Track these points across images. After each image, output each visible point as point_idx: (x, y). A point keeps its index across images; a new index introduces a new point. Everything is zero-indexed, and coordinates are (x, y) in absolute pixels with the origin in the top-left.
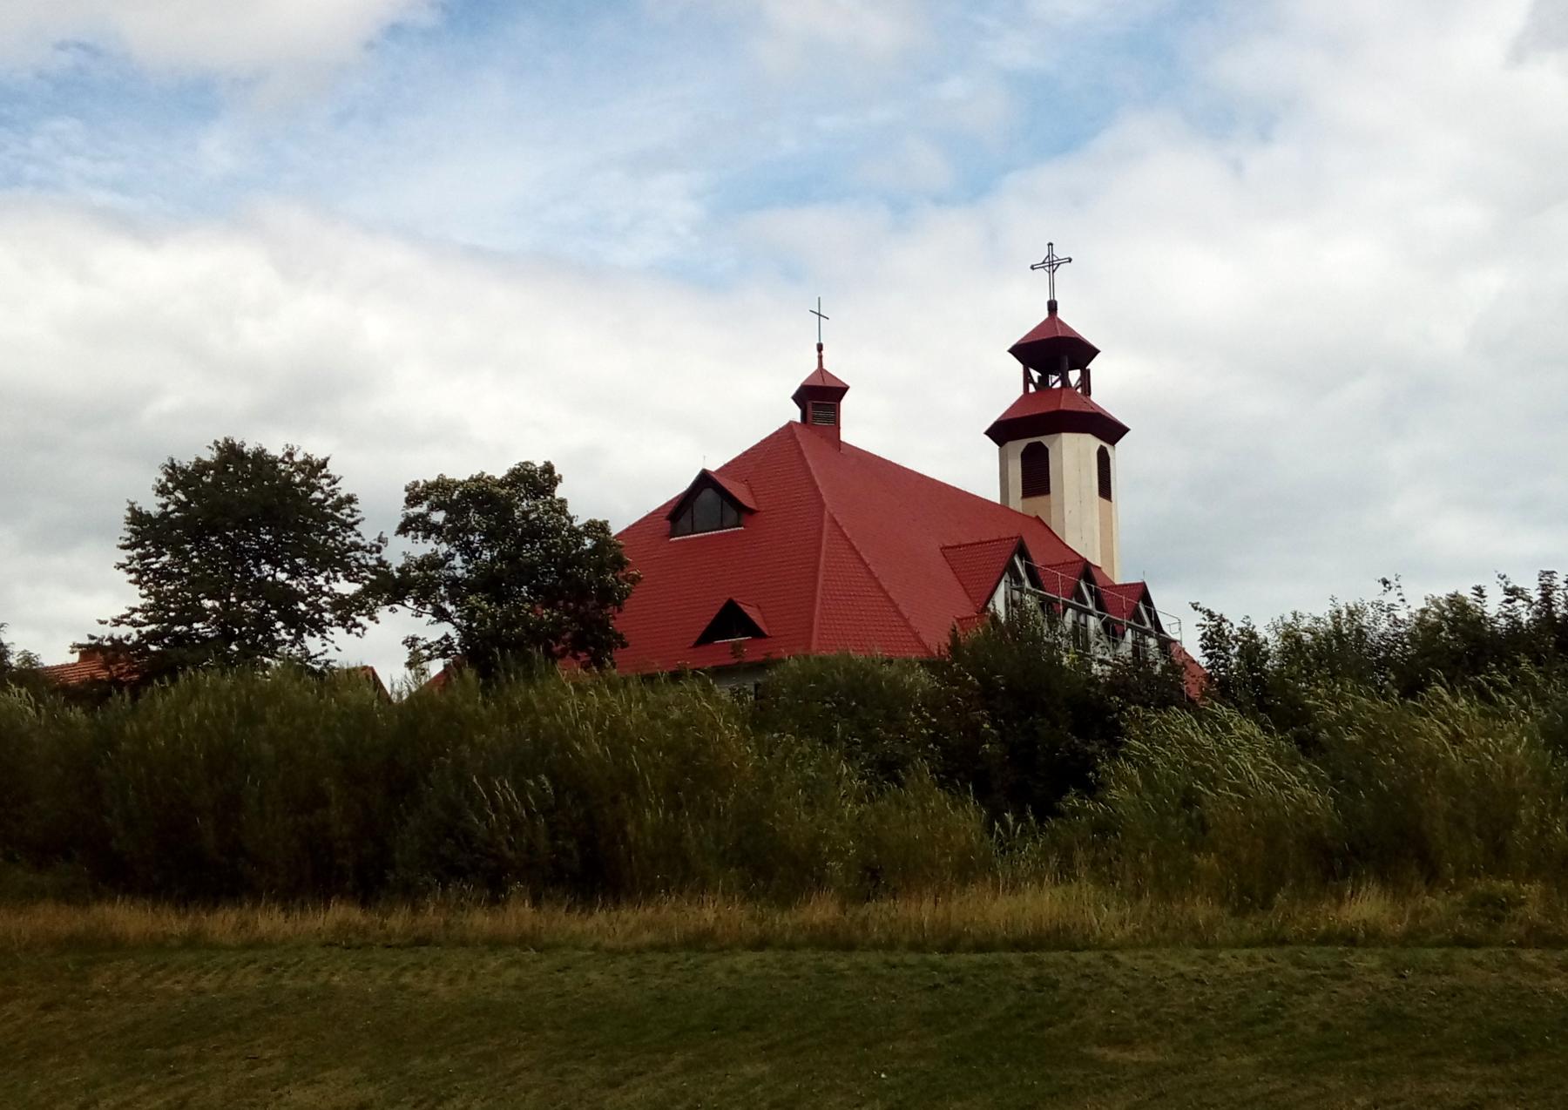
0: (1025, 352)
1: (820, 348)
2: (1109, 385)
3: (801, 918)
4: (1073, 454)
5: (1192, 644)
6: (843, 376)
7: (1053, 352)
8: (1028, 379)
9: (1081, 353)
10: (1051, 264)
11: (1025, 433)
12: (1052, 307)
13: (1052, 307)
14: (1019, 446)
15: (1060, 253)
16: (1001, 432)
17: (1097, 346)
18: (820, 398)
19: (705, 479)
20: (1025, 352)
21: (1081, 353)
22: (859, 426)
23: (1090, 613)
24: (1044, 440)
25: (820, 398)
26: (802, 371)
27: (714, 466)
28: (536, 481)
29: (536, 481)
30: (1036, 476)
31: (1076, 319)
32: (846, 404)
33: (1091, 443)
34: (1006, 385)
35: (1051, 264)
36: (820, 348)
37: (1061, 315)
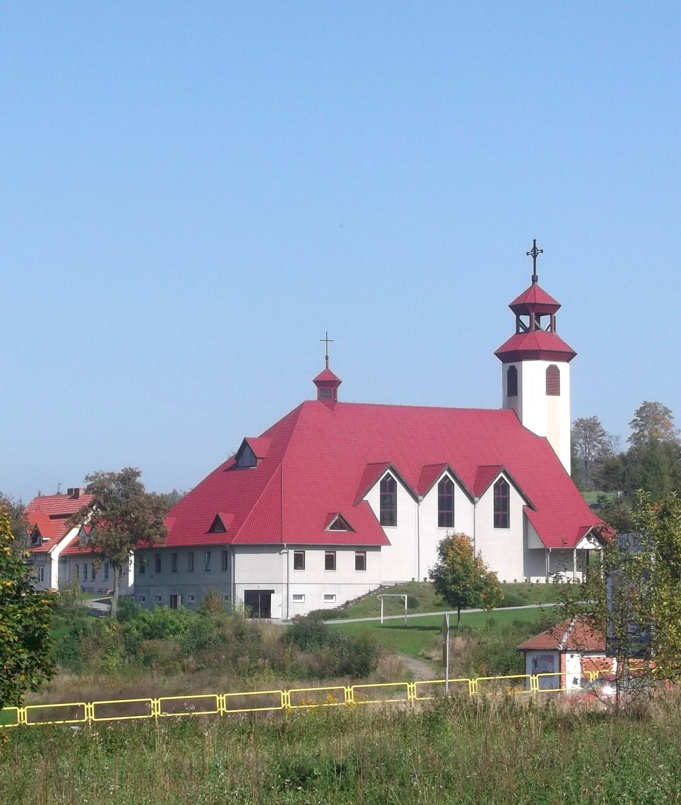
0: (519, 308)
1: (327, 358)
2: (567, 327)
4: (533, 372)
6: (339, 375)
7: (533, 306)
8: (519, 323)
9: (551, 308)
10: (535, 253)
11: (512, 356)
12: (535, 279)
13: (535, 279)
15: (539, 247)
17: (557, 298)
18: (327, 384)
20: (519, 308)
21: (551, 308)
22: (343, 395)
23: (83, 525)
25: (327, 384)
26: (318, 370)
27: (255, 432)
28: (128, 478)
29: (128, 478)
31: (550, 287)
32: (340, 389)
34: (505, 327)
35: (535, 253)
36: (327, 358)
37: (540, 283)
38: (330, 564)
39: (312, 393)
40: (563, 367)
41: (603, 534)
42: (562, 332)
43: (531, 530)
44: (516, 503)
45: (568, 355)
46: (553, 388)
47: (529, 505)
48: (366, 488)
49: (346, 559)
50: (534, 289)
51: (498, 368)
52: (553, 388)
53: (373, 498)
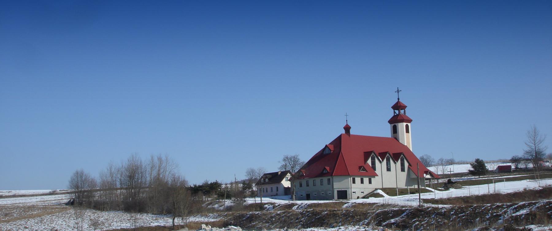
2: (409, 113)
3: (539, 228)
4: (402, 126)
5: (246, 199)
7: (398, 106)
8: (395, 112)
9: (404, 107)
10: (398, 91)
11: (395, 121)
12: (398, 99)
13: (398, 99)
14: (393, 125)
15: (399, 89)
16: (390, 122)
17: (406, 104)
18: (347, 129)
19: (326, 146)
21: (404, 107)
22: (352, 132)
24: (396, 124)
25: (347, 129)
27: (328, 144)
30: (395, 130)
31: (403, 101)
33: (405, 124)
34: (391, 114)
35: (398, 91)
38: (362, 182)
39: (343, 132)
40: (409, 124)
41: (39, 219)
42: (407, 114)
43: (411, 172)
44: (406, 164)
45: (410, 121)
46: (407, 131)
47: (410, 165)
48: (366, 160)
49: (366, 180)
50: (398, 102)
51: (389, 127)
52: (407, 131)
53: (369, 162)
